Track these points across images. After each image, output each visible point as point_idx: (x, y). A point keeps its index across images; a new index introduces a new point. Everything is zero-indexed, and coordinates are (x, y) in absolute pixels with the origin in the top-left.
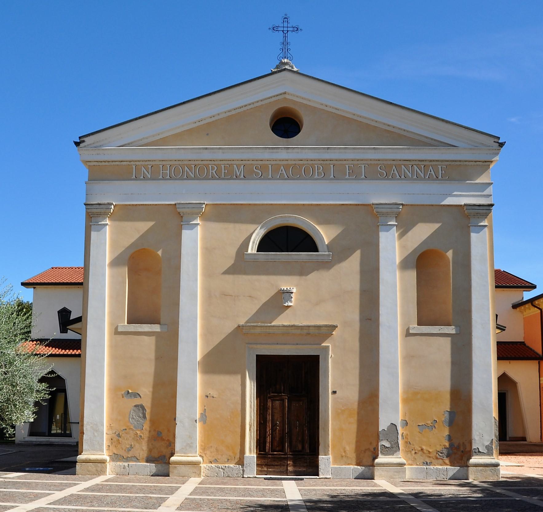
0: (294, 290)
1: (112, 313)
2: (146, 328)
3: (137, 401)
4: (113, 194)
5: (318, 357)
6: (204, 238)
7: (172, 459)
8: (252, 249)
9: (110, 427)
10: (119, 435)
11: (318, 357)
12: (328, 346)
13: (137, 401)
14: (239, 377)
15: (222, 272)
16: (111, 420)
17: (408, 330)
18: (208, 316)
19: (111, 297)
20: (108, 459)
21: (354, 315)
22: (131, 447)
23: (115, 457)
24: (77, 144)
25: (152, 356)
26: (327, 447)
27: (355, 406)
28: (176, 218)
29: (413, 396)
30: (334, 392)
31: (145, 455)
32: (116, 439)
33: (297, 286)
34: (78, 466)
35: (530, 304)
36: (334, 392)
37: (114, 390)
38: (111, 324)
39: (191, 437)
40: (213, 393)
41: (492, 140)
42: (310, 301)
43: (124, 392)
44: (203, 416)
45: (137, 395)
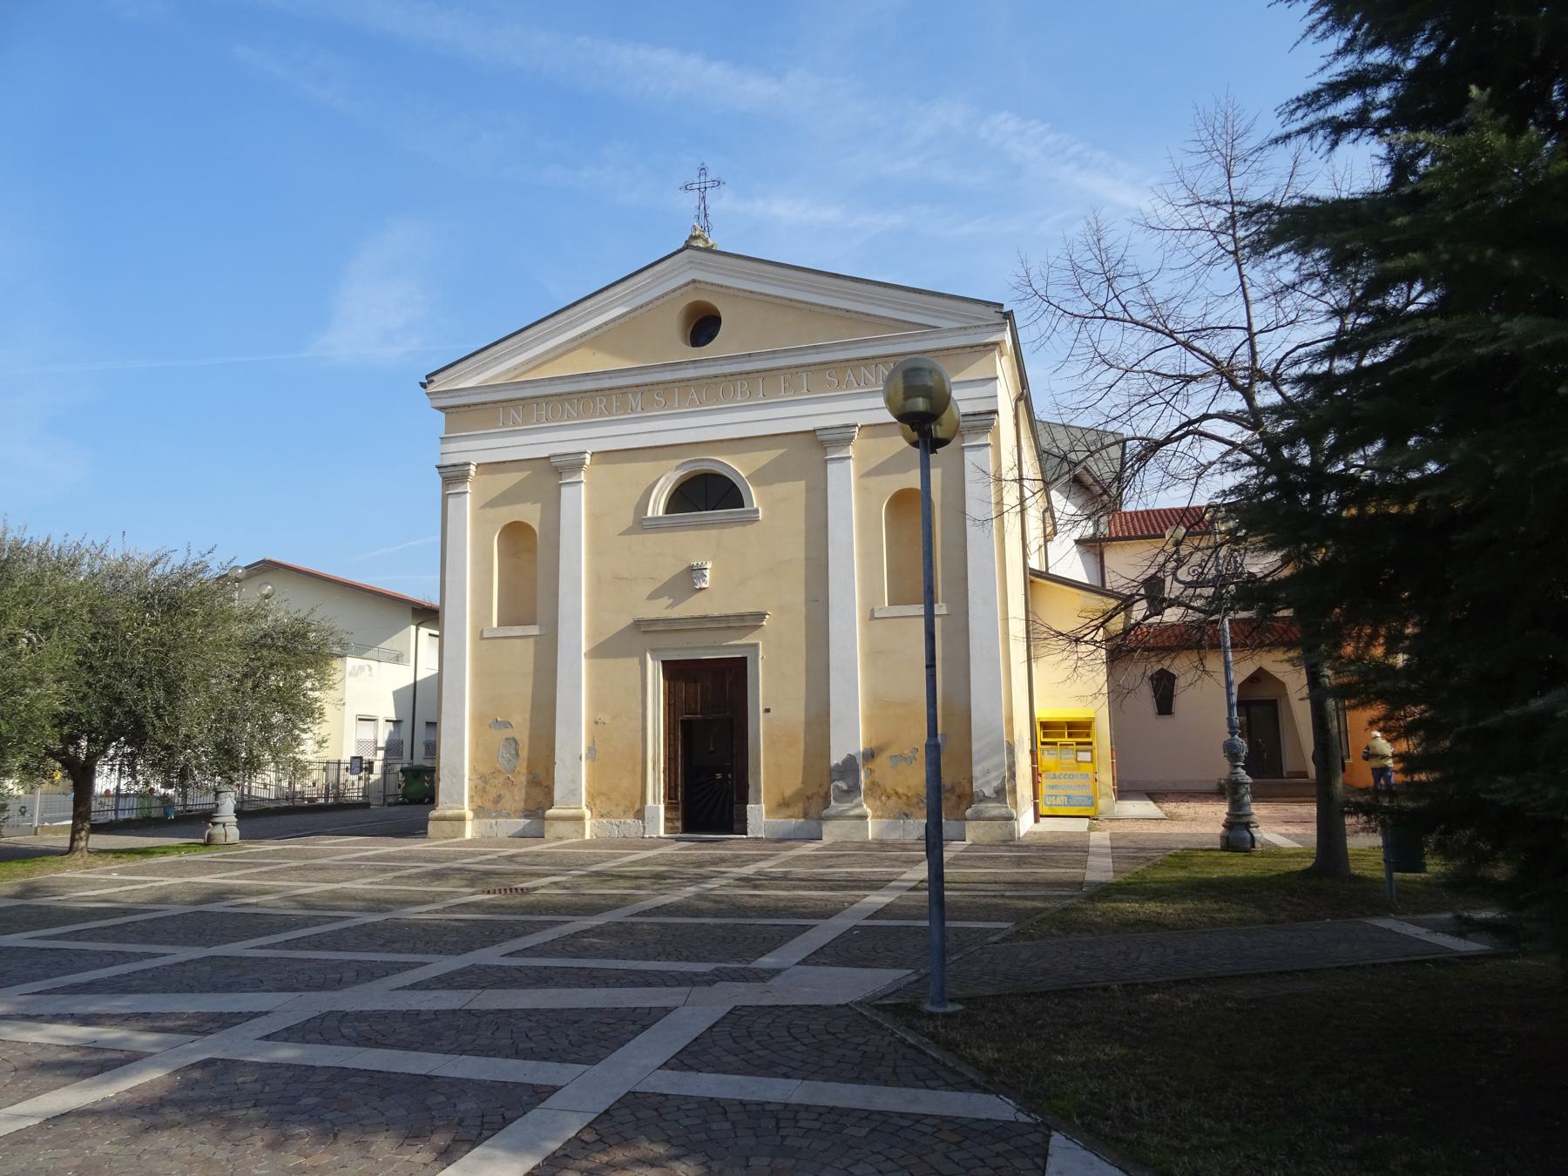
0: (709, 566)
1: (474, 613)
2: (518, 631)
3: (508, 733)
4: (475, 450)
5: (744, 659)
6: (590, 502)
7: (549, 812)
8: (657, 506)
9: (474, 769)
10: (486, 782)
11: (744, 659)
12: (756, 645)
13: (508, 733)
14: (636, 660)
15: (553, 1101)
16: (474, 760)
17: (872, 611)
18: (595, 611)
19: (474, 591)
20: (469, 815)
21: (795, 595)
22: (500, 797)
23: (479, 812)
24: (423, 385)
25: (530, 667)
26: (758, 791)
27: (800, 731)
28: (559, 469)
29: (880, 706)
30: (767, 711)
31: (521, 805)
32: (480, 790)
33: (713, 559)
34: (431, 826)
35: (1108, 586)
36: (767, 711)
37: (478, 718)
38: (474, 627)
39: (575, 781)
40: (606, 718)
41: (992, 310)
42: (729, 569)
43: (489, 722)
44: (591, 750)
45: (507, 725)
